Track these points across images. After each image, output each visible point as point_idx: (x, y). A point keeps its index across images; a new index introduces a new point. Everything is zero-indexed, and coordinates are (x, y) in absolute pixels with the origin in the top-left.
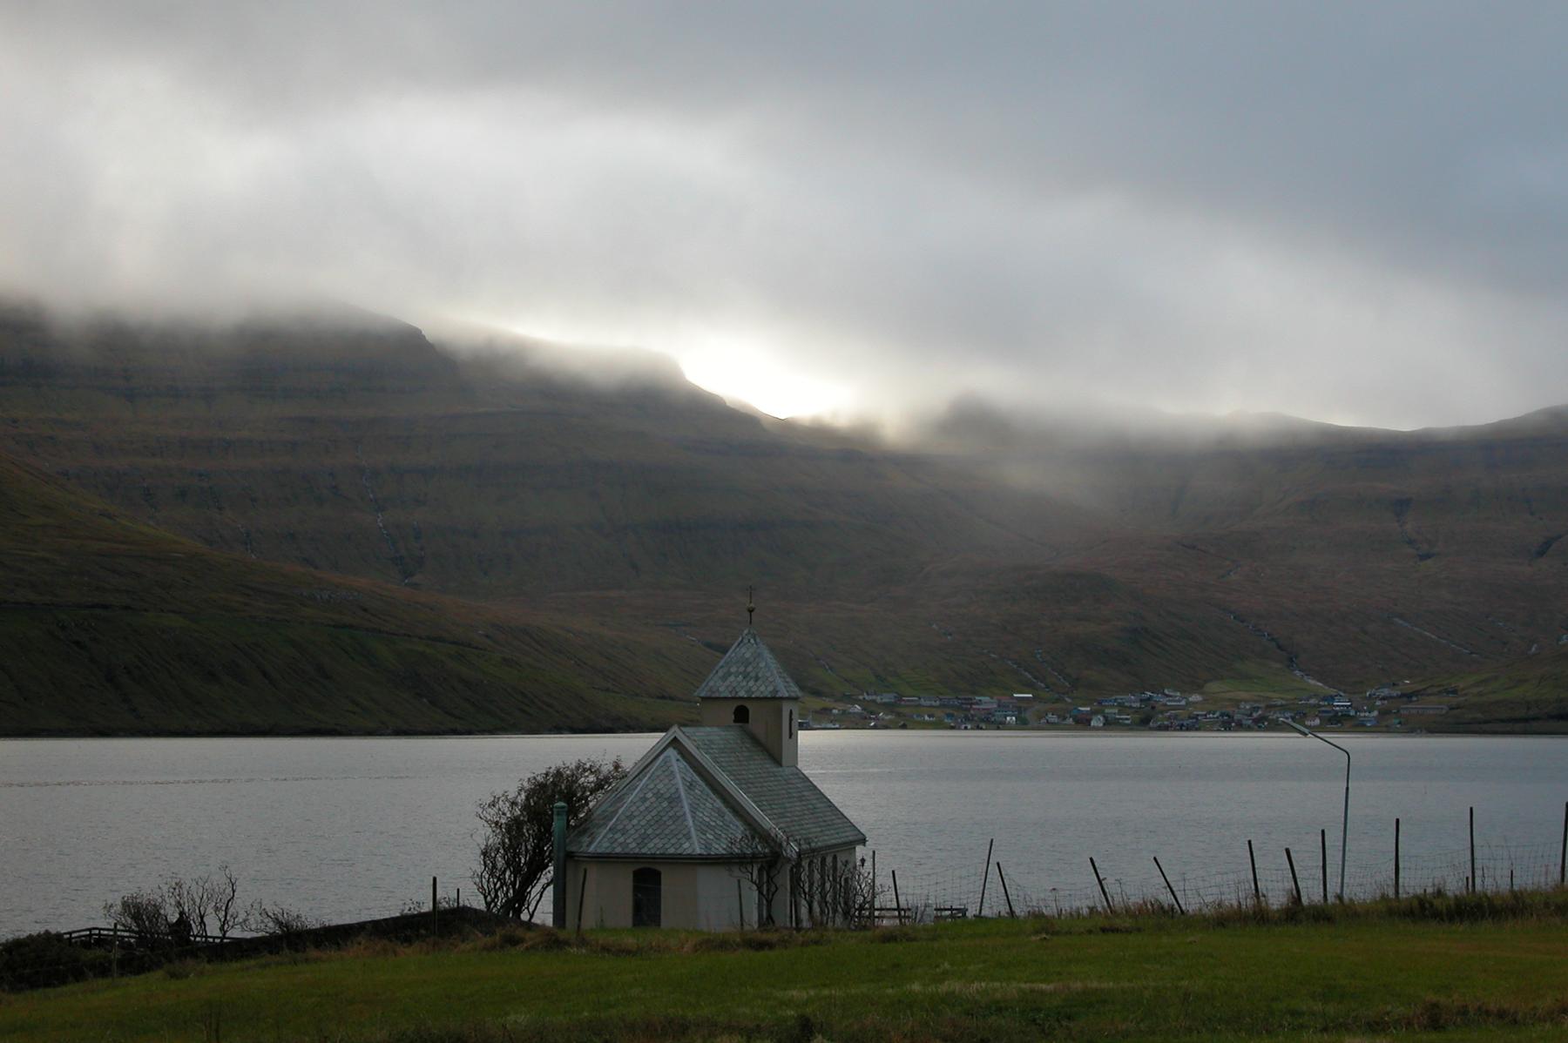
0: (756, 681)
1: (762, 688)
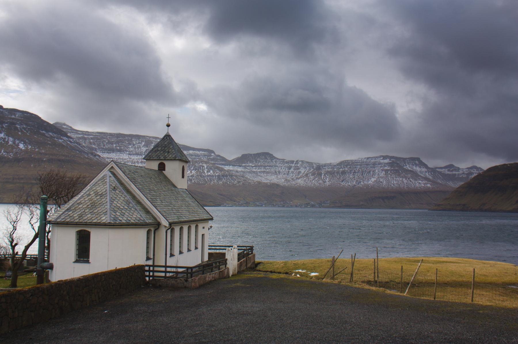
0: (168, 153)
1: (170, 156)
